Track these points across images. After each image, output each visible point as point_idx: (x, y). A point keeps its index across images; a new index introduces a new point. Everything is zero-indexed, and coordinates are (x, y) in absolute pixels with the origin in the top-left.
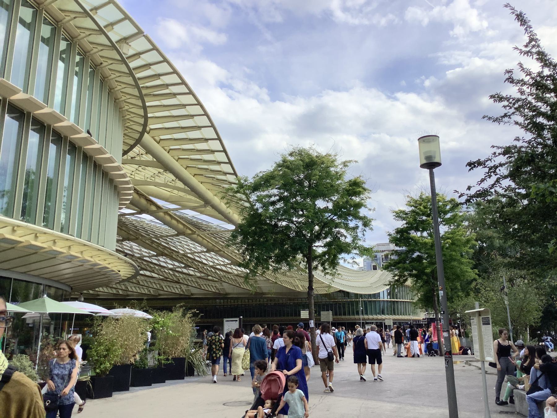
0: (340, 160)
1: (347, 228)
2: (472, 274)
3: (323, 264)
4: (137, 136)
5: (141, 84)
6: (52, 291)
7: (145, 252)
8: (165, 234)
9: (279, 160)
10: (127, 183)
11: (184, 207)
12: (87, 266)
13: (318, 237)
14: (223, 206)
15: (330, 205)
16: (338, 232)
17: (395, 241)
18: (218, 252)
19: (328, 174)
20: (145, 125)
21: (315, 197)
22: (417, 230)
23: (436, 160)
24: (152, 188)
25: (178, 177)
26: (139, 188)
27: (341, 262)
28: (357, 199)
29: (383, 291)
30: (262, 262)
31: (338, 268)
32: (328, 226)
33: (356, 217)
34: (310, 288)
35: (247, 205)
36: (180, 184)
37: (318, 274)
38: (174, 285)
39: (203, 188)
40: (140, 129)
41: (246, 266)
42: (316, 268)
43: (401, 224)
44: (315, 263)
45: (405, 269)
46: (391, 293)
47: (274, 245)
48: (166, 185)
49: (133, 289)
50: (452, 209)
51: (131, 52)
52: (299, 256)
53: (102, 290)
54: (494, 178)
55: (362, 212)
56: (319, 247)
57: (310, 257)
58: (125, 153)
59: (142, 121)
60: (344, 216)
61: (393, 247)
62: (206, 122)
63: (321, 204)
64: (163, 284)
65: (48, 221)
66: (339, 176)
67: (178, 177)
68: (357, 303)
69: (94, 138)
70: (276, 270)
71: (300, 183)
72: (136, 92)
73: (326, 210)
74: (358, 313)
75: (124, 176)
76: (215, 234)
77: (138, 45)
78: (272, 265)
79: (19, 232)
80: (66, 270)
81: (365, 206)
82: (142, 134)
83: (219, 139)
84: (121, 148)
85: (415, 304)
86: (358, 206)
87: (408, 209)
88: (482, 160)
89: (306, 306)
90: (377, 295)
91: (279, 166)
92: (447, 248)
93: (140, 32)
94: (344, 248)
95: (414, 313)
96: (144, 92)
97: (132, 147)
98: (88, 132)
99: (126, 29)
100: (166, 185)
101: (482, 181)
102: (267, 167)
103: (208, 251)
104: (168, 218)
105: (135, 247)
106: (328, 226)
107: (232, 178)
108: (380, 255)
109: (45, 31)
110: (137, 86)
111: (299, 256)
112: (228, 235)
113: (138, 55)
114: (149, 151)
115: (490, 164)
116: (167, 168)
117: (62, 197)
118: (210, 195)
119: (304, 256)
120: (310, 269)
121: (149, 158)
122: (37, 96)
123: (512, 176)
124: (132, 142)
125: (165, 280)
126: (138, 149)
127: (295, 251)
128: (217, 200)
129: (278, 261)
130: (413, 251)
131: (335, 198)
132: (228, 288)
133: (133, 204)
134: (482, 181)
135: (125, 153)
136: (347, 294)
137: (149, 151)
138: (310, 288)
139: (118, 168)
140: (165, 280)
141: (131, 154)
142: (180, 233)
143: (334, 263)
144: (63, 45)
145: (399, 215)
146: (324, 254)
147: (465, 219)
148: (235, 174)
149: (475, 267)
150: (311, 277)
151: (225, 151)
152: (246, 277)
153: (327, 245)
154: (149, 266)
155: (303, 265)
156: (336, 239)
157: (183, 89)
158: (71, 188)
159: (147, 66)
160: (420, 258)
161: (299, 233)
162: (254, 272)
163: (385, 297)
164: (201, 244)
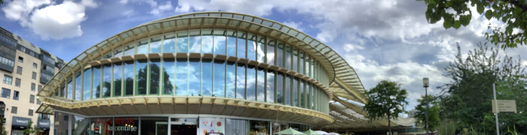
0: (398, 84)
1: (400, 104)
2: (438, 119)
3: (393, 116)
4: (333, 79)
5: (333, 64)
6: (312, 127)
7: (338, 114)
8: (343, 108)
9: (377, 84)
10: (330, 92)
11: (348, 99)
12: (321, 120)
13: (391, 108)
14: (360, 98)
15: (395, 98)
16: (398, 106)
17: (416, 108)
18: (360, 113)
19: (394, 88)
20: (335, 76)
21: (390, 94)
22: (424, 105)
23: (427, 85)
24: (339, 94)
25: (346, 90)
26: (335, 94)
27: (399, 116)
28: (403, 96)
29: (413, 125)
30: (373, 116)
31: (399, 118)
32: (394, 105)
33: (404, 101)
34: (389, 125)
35: (368, 98)
36: (346, 92)
37: (392, 120)
38: (347, 124)
39: (354, 93)
40: (333, 77)
41: (369, 118)
42: (391, 118)
43: (419, 103)
44: (391, 116)
45: (420, 118)
46: (416, 125)
47: (377, 111)
48: (342, 93)
49: (336, 126)
50: (434, 100)
51: (329, 56)
52: (385, 114)
53: (327, 126)
54: (444, 92)
55: (406, 100)
56: (392, 111)
57: (389, 114)
58: (330, 84)
59: (334, 75)
60: (400, 101)
61: (417, 111)
62: (354, 73)
63: (392, 97)
64: (344, 124)
65: (309, 107)
66: (397, 89)
67: (346, 90)
68: (405, 129)
69: (319, 82)
70: (378, 119)
71: (385, 91)
72: (331, 67)
73: (394, 99)
74: (405, 132)
75: (330, 91)
76: (359, 107)
77: (331, 53)
78: (377, 117)
79: (301, 111)
80: (316, 121)
81: (407, 98)
82: (334, 78)
83: (358, 78)
84: (328, 83)
85: (423, 129)
86: (404, 98)
87: (421, 99)
88: (440, 86)
89: (388, 131)
90: (412, 126)
91: (377, 86)
92: (433, 111)
93: (331, 50)
94: (400, 111)
95: (422, 131)
96: (334, 66)
97: (331, 83)
98: (317, 80)
99: (327, 50)
100: (342, 93)
101: (441, 93)
102: (374, 86)
103: (357, 113)
104: (344, 103)
105: (334, 112)
106: (394, 105)
107: (363, 90)
108: (413, 113)
109: (307, 58)
110: (332, 65)
111: (385, 114)
112: (362, 108)
113: (331, 56)
114: (337, 83)
115: (443, 88)
116: (342, 87)
117: (312, 98)
118: (356, 95)
119: (387, 114)
120: (389, 118)
121: (337, 85)
122: (308, 76)
123: (449, 92)
124: (331, 81)
125: (344, 123)
126: (333, 83)
127: (384, 113)
128: (359, 97)
129: (379, 116)
130: (422, 112)
131: (397, 95)
132: (364, 125)
133: (333, 99)
134: (441, 93)
135: (330, 84)
136: (402, 126)
137: (337, 83)
138: (389, 125)
139: (328, 89)
140: (344, 123)
141: (332, 84)
142: (348, 108)
143: (397, 116)
144: (312, 60)
145: (419, 100)
146: (393, 113)
147: (438, 102)
148: (364, 88)
149: (440, 117)
150: (389, 121)
151: (360, 81)
152: (369, 122)
153: (395, 110)
154: (339, 118)
155: (387, 117)
156: (397, 109)
157: (346, 64)
158: (314, 97)
159: (334, 59)
160: (424, 114)
161: (385, 107)
162: (371, 120)
163: (414, 127)
164: (355, 111)
